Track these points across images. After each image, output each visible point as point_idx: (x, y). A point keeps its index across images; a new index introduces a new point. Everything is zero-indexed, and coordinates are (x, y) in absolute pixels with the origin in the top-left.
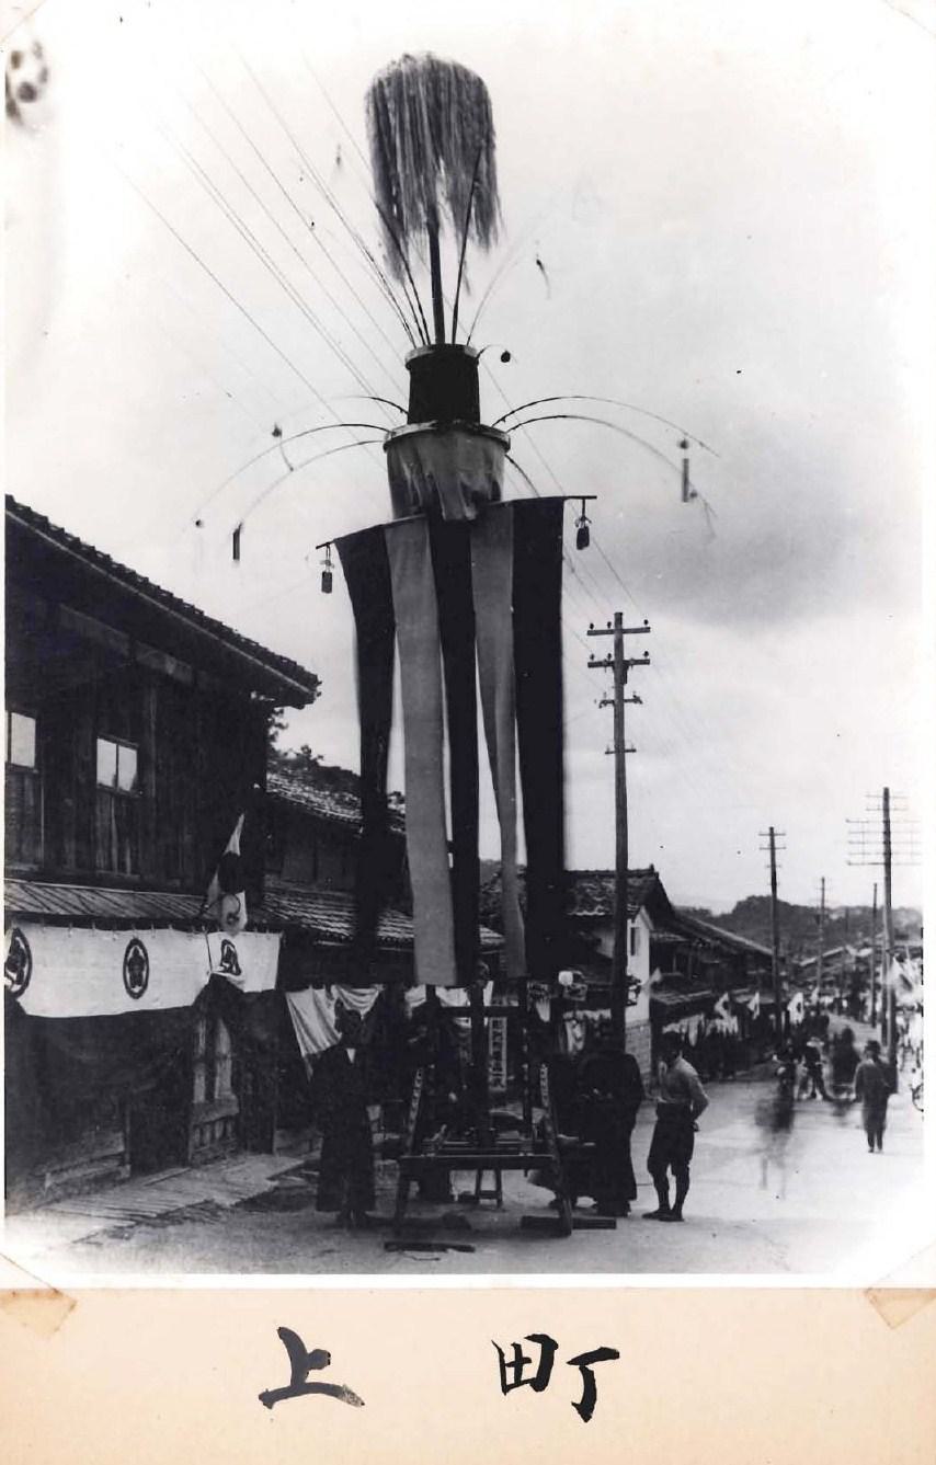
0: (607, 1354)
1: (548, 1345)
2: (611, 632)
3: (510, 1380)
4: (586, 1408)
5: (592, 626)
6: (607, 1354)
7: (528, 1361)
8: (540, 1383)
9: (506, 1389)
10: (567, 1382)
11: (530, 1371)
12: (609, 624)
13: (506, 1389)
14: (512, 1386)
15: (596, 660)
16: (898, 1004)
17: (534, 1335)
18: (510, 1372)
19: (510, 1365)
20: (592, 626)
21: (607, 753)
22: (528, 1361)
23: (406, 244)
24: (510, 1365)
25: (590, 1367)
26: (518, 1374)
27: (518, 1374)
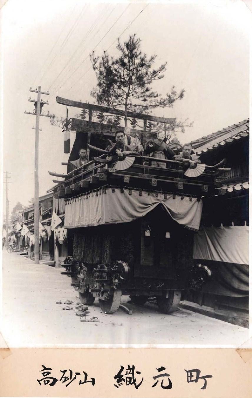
0: (209, 376)
1: (198, 371)
2: (37, 92)
3: (189, 380)
4: (204, 387)
5: (31, 88)
6: (209, 376)
7: (193, 376)
8: (196, 381)
9: (188, 382)
10: (201, 382)
11: (194, 378)
12: (36, 89)
13: (188, 382)
14: (83, 383)
15: (31, 99)
16: (51, 202)
17: (134, 367)
18: (189, 378)
19: (189, 376)
20: (31, 88)
21: (33, 128)
22: (193, 376)
23: (232, 254)
24: (189, 376)
25: (206, 379)
26: (191, 379)
27: (191, 379)
